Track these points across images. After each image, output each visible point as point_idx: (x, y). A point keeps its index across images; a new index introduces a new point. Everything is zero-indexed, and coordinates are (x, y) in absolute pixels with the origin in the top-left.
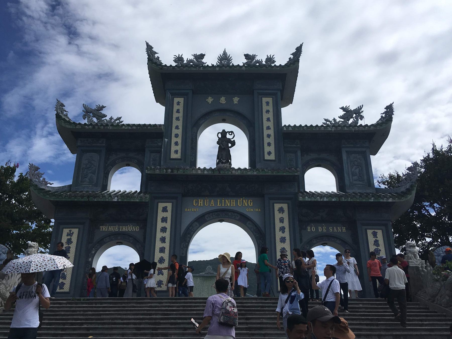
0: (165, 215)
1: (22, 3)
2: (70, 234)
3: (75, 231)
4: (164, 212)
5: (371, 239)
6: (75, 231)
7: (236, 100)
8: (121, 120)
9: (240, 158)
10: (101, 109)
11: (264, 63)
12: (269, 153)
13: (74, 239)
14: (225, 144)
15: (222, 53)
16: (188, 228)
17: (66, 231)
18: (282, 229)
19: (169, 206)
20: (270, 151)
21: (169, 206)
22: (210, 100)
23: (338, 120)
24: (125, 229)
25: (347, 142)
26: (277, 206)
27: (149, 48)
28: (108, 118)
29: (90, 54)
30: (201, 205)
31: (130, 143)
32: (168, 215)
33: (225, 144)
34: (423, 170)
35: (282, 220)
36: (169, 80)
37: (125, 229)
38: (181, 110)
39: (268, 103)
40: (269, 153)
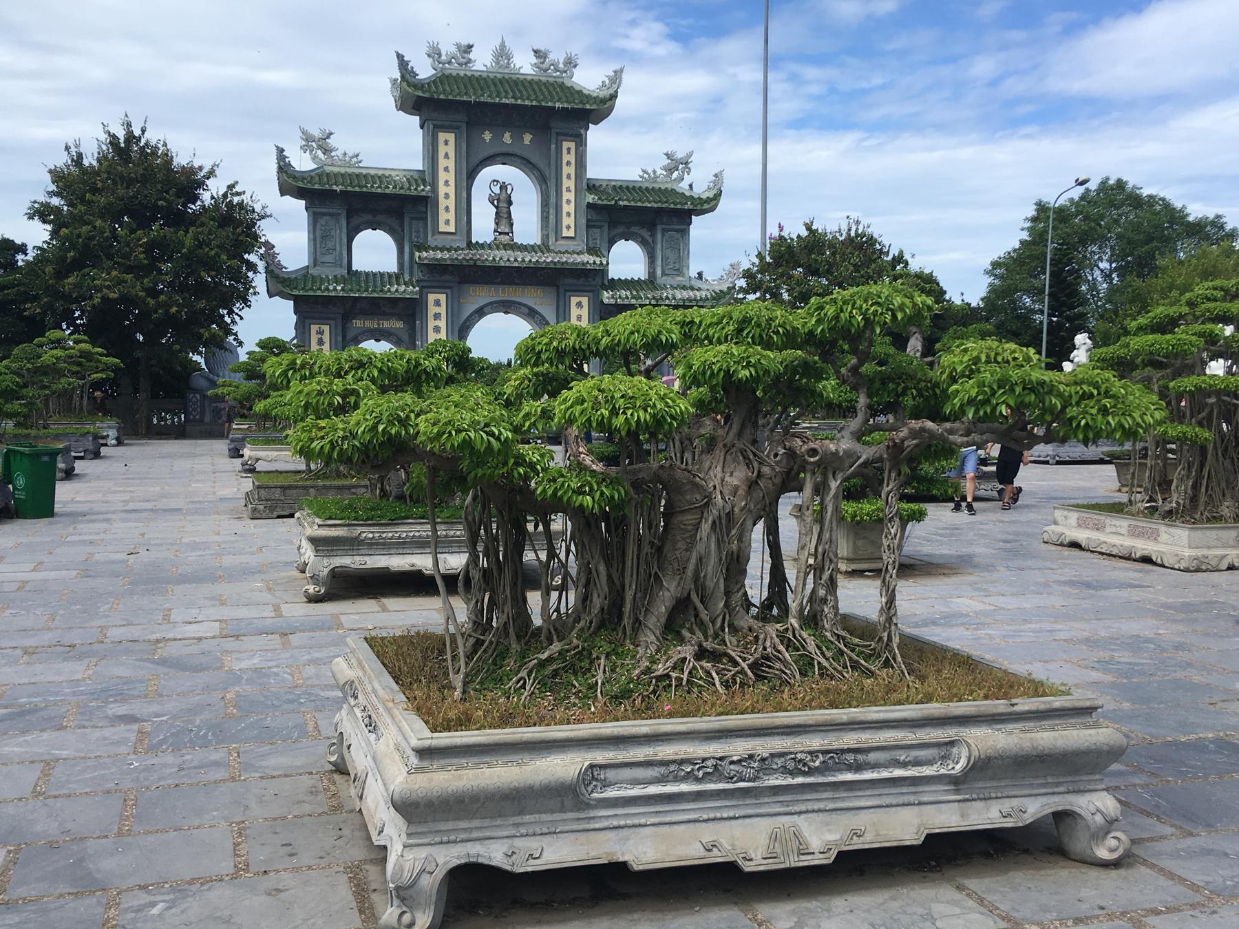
0: (437, 310)
2: (322, 333)
3: (326, 328)
4: (437, 304)
6: (326, 328)
7: (527, 138)
8: (360, 158)
9: (527, 225)
10: (328, 137)
11: (561, 66)
12: (568, 227)
13: (326, 338)
14: (503, 204)
15: (498, 43)
16: (468, 319)
17: (314, 328)
19: (442, 298)
21: (442, 298)
22: (487, 136)
23: (659, 172)
24: (386, 324)
25: (657, 215)
26: (574, 300)
27: (400, 57)
28: (339, 153)
29: (962, 615)
30: (479, 296)
31: (400, 207)
32: (442, 310)
33: (503, 204)
37: (386, 324)
39: (569, 150)
40: (568, 227)
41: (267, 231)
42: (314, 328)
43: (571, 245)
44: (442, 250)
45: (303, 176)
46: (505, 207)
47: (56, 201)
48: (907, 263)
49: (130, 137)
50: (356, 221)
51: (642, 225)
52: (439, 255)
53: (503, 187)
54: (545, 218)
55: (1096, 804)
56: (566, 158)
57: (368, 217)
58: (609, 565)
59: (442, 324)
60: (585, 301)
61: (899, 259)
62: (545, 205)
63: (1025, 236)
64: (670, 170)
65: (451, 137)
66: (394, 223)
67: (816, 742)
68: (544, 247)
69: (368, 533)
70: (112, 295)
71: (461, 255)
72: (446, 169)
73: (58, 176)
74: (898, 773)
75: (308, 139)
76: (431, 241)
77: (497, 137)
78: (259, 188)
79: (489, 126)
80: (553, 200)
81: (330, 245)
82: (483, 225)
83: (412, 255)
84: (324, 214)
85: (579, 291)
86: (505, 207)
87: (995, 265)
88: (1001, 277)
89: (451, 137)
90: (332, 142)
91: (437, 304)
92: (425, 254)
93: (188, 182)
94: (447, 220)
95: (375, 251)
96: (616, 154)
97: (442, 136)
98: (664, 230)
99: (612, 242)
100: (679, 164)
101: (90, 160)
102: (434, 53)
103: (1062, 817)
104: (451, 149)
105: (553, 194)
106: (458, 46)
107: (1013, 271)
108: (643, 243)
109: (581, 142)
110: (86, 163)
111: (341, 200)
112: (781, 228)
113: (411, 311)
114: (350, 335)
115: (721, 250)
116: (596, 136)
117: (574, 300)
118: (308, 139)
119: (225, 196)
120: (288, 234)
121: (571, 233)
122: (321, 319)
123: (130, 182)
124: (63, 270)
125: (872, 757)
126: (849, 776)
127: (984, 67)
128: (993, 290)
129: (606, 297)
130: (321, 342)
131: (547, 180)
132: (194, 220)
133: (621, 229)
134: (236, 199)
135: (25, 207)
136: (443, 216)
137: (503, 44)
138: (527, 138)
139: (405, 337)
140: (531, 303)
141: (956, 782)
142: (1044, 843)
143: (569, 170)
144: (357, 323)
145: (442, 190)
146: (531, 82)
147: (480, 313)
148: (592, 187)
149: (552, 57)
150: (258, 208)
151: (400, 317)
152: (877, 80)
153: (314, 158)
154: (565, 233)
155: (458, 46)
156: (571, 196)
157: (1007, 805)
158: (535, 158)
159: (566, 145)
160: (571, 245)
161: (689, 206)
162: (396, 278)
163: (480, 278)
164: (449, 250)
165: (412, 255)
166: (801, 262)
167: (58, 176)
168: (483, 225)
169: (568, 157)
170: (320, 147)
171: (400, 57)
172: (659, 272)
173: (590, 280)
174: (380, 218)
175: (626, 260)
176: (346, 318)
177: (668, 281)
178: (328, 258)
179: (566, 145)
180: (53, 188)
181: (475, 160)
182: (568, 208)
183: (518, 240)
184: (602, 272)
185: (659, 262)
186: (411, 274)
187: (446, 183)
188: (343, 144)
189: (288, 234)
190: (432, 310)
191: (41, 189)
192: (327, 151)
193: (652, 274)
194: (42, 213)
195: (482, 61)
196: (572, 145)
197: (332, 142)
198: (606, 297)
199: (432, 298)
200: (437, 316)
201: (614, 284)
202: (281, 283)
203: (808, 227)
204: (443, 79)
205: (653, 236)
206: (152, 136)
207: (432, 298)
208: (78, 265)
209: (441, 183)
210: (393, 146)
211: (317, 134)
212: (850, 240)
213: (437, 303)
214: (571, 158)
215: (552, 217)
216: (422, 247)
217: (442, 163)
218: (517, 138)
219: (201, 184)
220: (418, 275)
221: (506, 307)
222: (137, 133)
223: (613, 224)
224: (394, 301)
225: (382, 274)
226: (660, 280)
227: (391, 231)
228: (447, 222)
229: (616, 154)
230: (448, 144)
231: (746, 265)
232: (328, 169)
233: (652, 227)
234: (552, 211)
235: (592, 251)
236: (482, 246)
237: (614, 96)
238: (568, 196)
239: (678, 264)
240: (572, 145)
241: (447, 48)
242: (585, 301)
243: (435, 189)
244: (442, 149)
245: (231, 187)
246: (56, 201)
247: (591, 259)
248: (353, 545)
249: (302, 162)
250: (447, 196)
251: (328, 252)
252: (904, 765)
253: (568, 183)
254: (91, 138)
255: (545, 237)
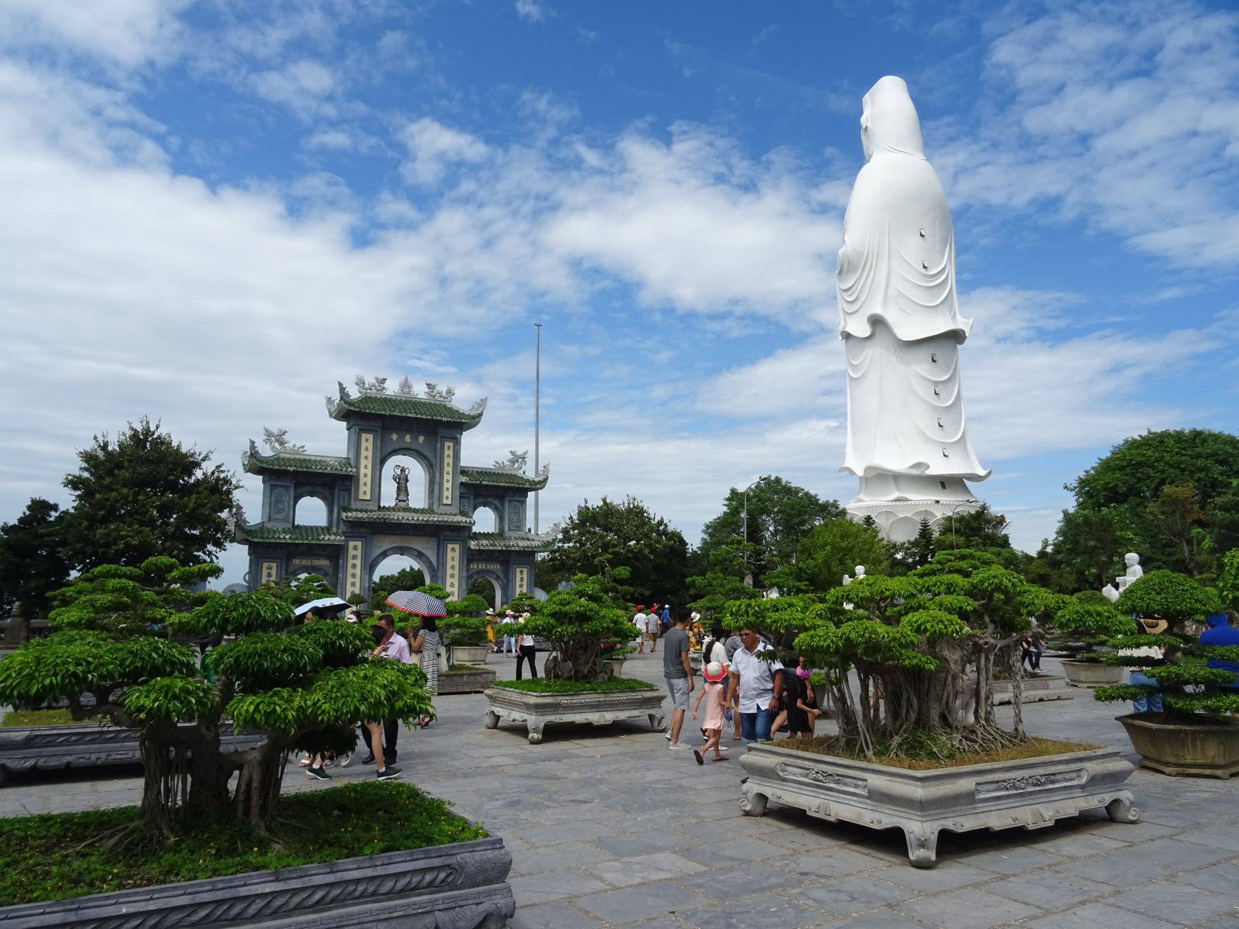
0: (355, 553)
1: (851, 184)
2: (270, 568)
3: (274, 565)
4: (355, 549)
5: (518, 576)
6: (274, 565)
7: (421, 439)
9: (418, 497)
14: (402, 482)
17: (265, 565)
18: (453, 567)
19: (359, 544)
20: (448, 492)
21: (359, 544)
22: (394, 437)
24: (317, 563)
25: (504, 491)
26: (450, 546)
27: (340, 384)
28: (291, 445)
30: (385, 543)
31: (330, 482)
32: (359, 552)
33: (402, 482)
34: (860, 569)
35: (453, 559)
36: (362, 415)
37: (317, 563)
38: (370, 448)
41: (237, 495)
42: (265, 565)
43: (449, 510)
44: (361, 511)
45: (266, 460)
46: (403, 483)
47: (86, 475)
48: (666, 525)
49: (147, 432)
50: (301, 490)
51: (495, 497)
52: (360, 515)
53: (403, 470)
54: (431, 491)
55: (1126, 795)
56: (447, 452)
57: (309, 488)
58: (919, 699)
59: (358, 562)
60: (457, 547)
61: (661, 523)
62: (432, 482)
63: (725, 509)
64: (513, 462)
65: (370, 437)
66: (497, 503)
67: (1041, 771)
68: (430, 511)
69: (564, 700)
70: (134, 542)
71: (375, 515)
72: (367, 449)
73: (89, 457)
74: (1066, 784)
75: (269, 434)
76: (353, 505)
77: (401, 438)
78: (234, 468)
79: (397, 430)
80: (437, 479)
81: (281, 507)
82: (388, 497)
83: (339, 514)
84: (277, 486)
85: (453, 541)
86: (403, 483)
87: (708, 527)
88: (710, 534)
89: (370, 437)
90: (286, 437)
91: (355, 549)
92: (350, 514)
93: (187, 464)
94: (365, 491)
95: (312, 511)
96: (480, 450)
97: (364, 436)
98: (510, 501)
99: (475, 508)
100: (518, 459)
101: (113, 446)
102: (360, 383)
103: (1116, 802)
104: (370, 445)
105: (438, 475)
106: (377, 379)
107: (720, 529)
108: (495, 509)
109: (457, 442)
110: (110, 448)
111: (288, 476)
112: (586, 501)
113: (336, 554)
114: (291, 569)
115: (548, 516)
116: (467, 438)
117: (450, 546)
118: (269, 434)
119: (213, 473)
120: (251, 497)
121: (449, 502)
122: (271, 559)
123: (147, 461)
124: (93, 521)
125: (1058, 777)
126: (1051, 786)
127: (660, 392)
128: (704, 542)
129: (473, 544)
130: (269, 575)
131: (433, 466)
132: (188, 490)
133: (481, 500)
134: (222, 476)
135: (62, 478)
136: (362, 488)
137: (406, 380)
138: (421, 439)
139: (330, 571)
140: (419, 547)
141: (1082, 787)
142: (1110, 816)
143: (448, 460)
144: (296, 562)
145: (363, 471)
146: (425, 404)
147: (385, 555)
148: (464, 472)
149: (438, 388)
150: (234, 482)
151: (327, 557)
152: (593, 397)
153: (273, 448)
154: (445, 502)
155: (377, 379)
156: (450, 477)
157: (1099, 797)
158: (426, 452)
159: (447, 444)
160: (449, 510)
161: (527, 486)
162: (328, 530)
163: (382, 530)
164: (366, 511)
165: (339, 514)
166: (597, 520)
167: (89, 457)
168: (388, 497)
169: (448, 452)
170: (277, 441)
171: (340, 384)
172: (506, 528)
173: (461, 533)
174: (317, 489)
175: (484, 520)
176: (290, 557)
177: (513, 534)
178: (279, 516)
179: (447, 444)
180: (84, 465)
181: (385, 453)
182: (448, 485)
183: (412, 505)
184: (468, 528)
185: (506, 522)
186: (338, 528)
187: (366, 467)
188: (292, 441)
189: (251, 497)
190: (351, 552)
191: (76, 467)
192: (282, 443)
193: (501, 530)
194: (74, 483)
195: (392, 388)
196: (451, 444)
197: (286, 437)
198: (473, 544)
199: (351, 544)
200: (355, 557)
201: (477, 536)
202: (246, 535)
203: (604, 500)
204: (366, 399)
205: (502, 504)
206: (163, 431)
207: (351, 544)
208: (105, 521)
209: (362, 466)
210: (328, 441)
211: (276, 432)
212: (629, 511)
213: (453, 550)
214: (451, 452)
215: (436, 491)
216: (346, 509)
217: (363, 453)
218: (415, 438)
219: (197, 465)
220: (343, 528)
221: (402, 551)
222: (152, 428)
223: (476, 497)
224: (324, 547)
225: (317, 528)
226: (507, 534)
227: (324, 498)
228: (365, 493)
229: (480, 450)
230: (368, 441)
231: (563, 525)
232: (282, 455)
233: (501, 498)
234: (436, 487)
235: (463, 513)
236: (388, 509)
237: (480, 415)
238: (448, 477)
239: (519, 524)
240: (451, 444)
241: (370, 380)
242: (457, 547)
243: (358, 472)
244: (364, 444)
245: (218, 467)
246: (86, 475)
247: (464, 519)
248: (555, 707)
249: (266, 451)
250: (366, 475)
251: (279, 512)
252: (1066, 780)
253: (448, 469)
254: (115, 434)
255: (431, 504)
